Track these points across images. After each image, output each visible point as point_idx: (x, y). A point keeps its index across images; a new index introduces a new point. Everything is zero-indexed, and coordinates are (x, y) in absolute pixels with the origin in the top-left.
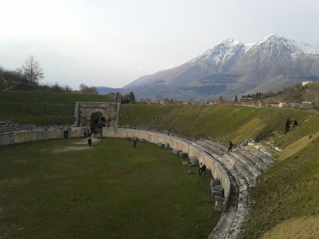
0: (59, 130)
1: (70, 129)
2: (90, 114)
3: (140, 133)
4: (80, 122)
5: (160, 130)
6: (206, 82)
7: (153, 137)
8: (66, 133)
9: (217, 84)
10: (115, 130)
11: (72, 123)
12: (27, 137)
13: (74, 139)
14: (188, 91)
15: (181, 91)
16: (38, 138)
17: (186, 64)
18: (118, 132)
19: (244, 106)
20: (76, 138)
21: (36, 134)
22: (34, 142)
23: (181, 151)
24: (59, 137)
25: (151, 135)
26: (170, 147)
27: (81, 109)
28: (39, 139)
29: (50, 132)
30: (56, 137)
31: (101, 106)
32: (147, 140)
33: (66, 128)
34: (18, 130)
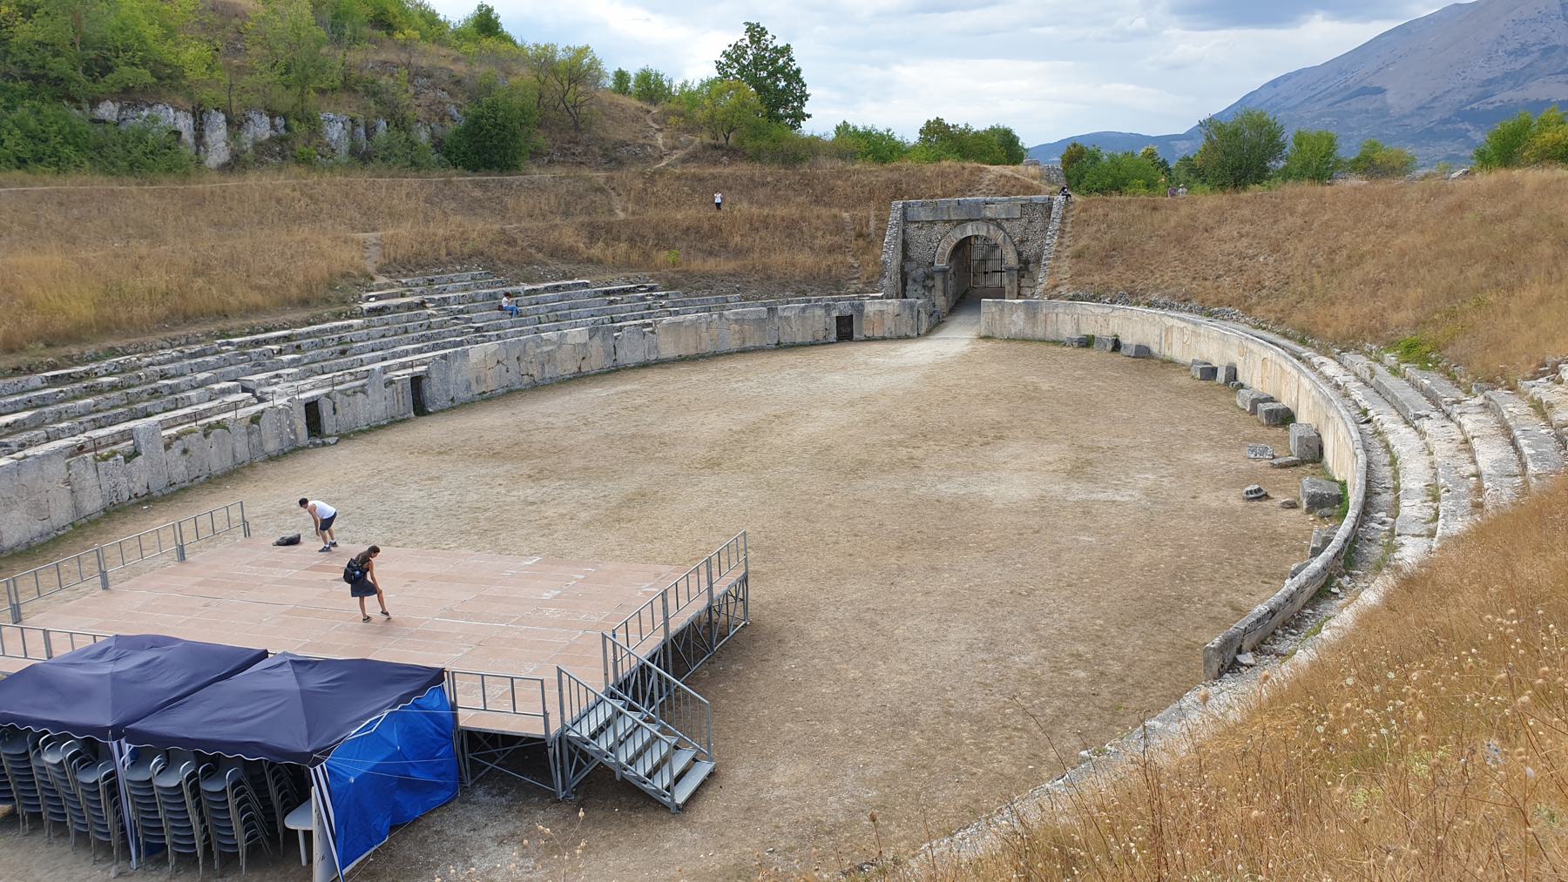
0: (819, 312)
1: (860, 309)
2: (946, 247)
4: (910, 282)
7: (1176, 335)
10: (1032, 311)
11: (871, 284)
18: (1041, 317)
19: (1367, 619)
23: (1271, 400)
24: (820, 336)
25: (1169, 330)
26: (1240, 378)
27: (917, 235)
28: (748, 344)
29: (787, 318)
31: (989, 214)
32: (1155, 349)
33: (843, 307)
34: (677, 313)
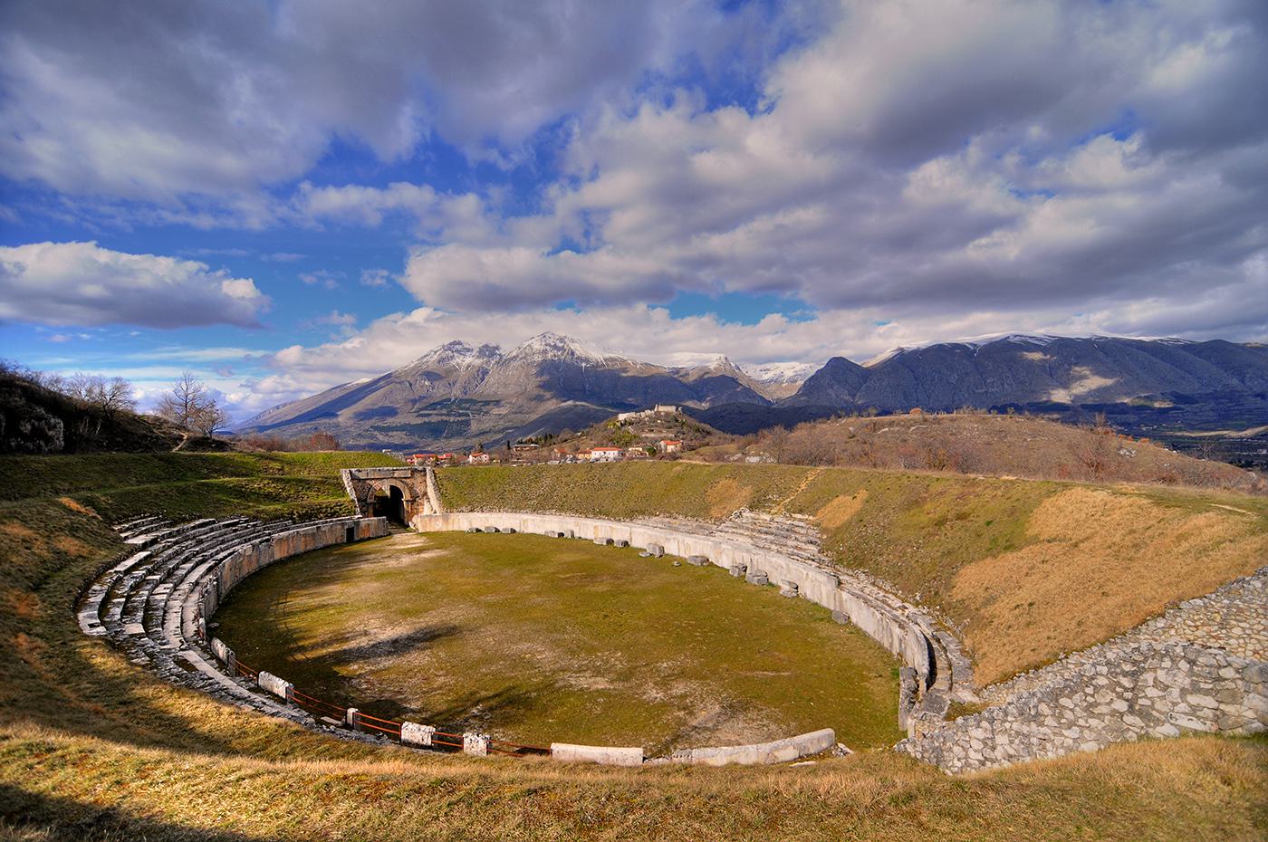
3: (501, 518)
5: (541, 507)
6: (429, 415)
8: (350, 532)
9: (452, 419)
10: (446, 520)
12: (291, 545)
13: (372, 541)
14: (390, 434)
15: (376, 433)
16: (306, 546)
17: (939, 345)
18: (451, 521)
20: (369, 539)
21: (303, 539)
22: (282, 562)
24: (339, 541)
28: (308, 547)
30: (334, 542)
